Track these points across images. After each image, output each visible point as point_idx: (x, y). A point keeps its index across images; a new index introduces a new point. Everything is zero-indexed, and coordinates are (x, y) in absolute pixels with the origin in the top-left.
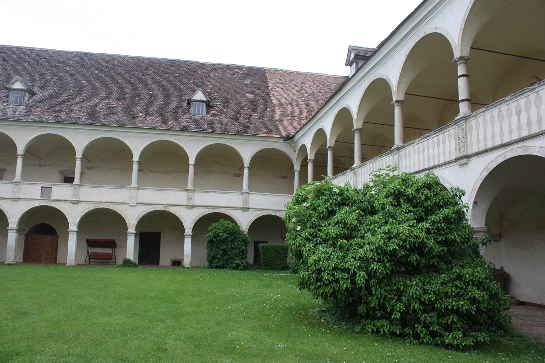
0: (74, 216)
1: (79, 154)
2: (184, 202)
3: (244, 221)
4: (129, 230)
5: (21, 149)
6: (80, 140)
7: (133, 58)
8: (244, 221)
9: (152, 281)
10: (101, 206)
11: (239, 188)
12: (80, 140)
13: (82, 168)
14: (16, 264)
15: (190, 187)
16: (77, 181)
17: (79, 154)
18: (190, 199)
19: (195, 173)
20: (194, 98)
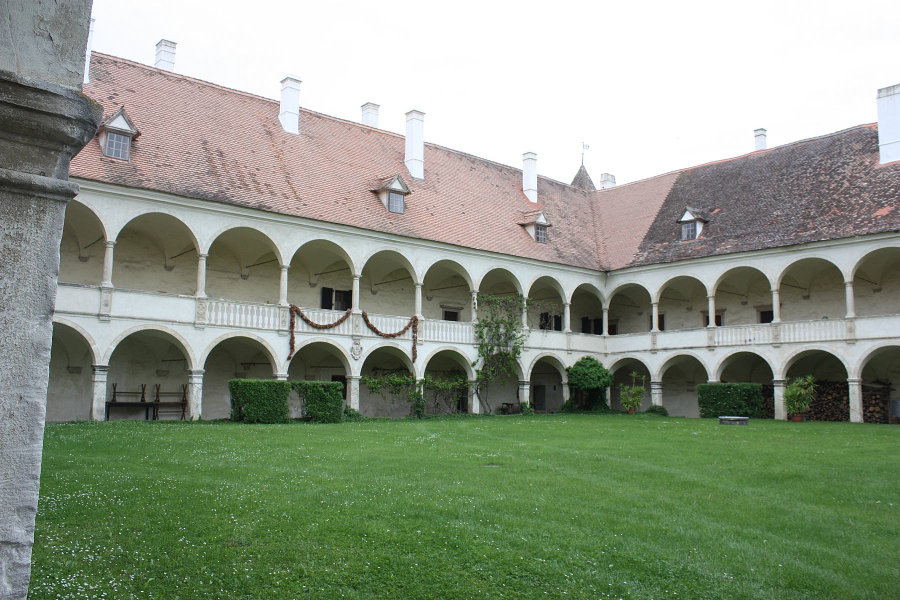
0: (779, 363)
1: (775, 285)
2: (649, 346)
3: (608, 364)
4: (850, 378)
5: (848, 275)
6: (773, 267)
7: (786, 147)
8: (608, 364)
9: (823, 442)
10: (625, 357)
11: (840, 314)
12: (773, 267)
13: (780, 300)
14: (783, 421)
15: (850, 314)
16: (776, 319)
17: (775, 285)
18: (711, 338)
19: (856, 295)
20: (683, 219)
